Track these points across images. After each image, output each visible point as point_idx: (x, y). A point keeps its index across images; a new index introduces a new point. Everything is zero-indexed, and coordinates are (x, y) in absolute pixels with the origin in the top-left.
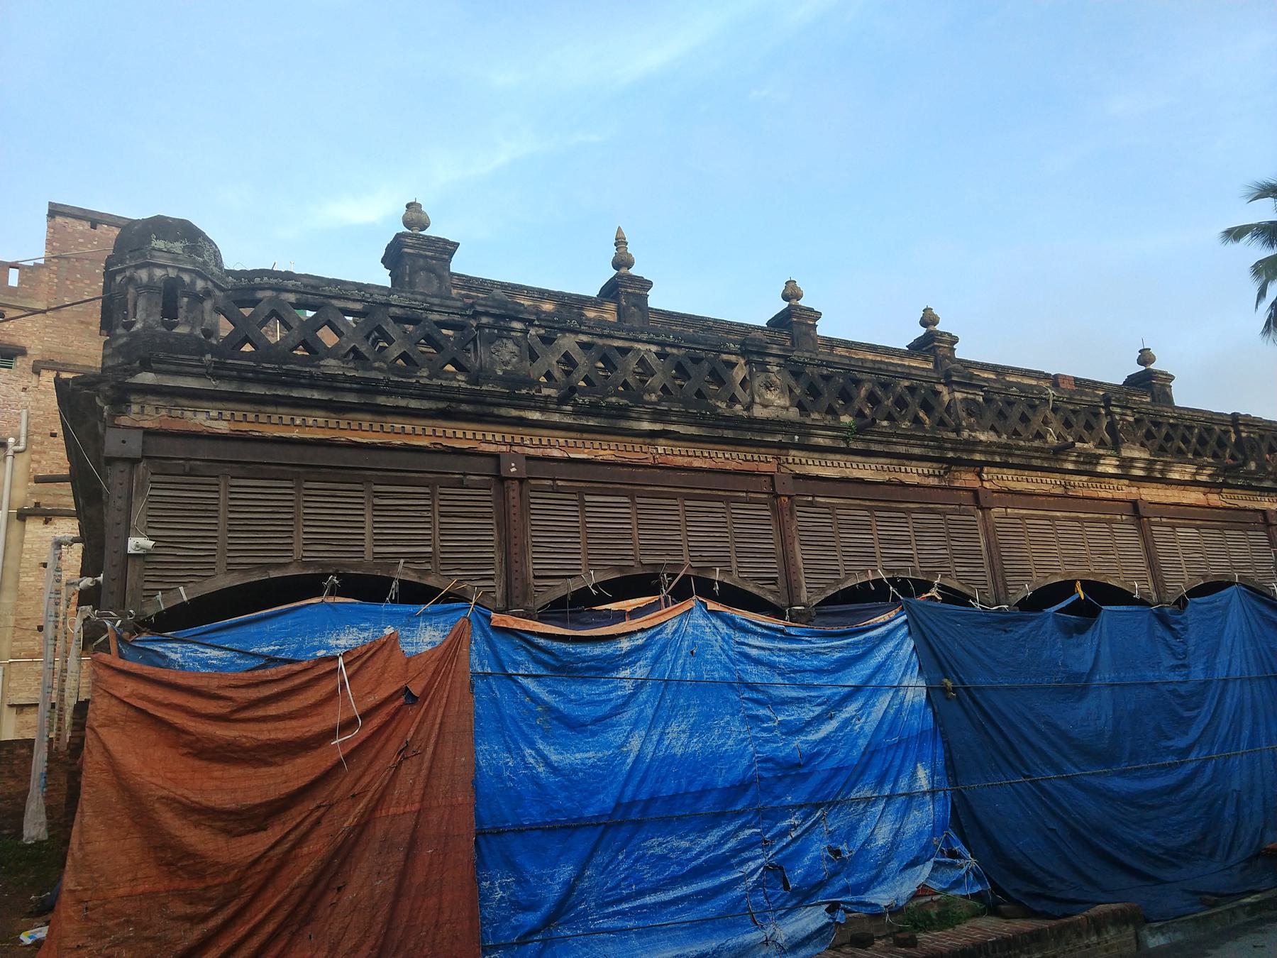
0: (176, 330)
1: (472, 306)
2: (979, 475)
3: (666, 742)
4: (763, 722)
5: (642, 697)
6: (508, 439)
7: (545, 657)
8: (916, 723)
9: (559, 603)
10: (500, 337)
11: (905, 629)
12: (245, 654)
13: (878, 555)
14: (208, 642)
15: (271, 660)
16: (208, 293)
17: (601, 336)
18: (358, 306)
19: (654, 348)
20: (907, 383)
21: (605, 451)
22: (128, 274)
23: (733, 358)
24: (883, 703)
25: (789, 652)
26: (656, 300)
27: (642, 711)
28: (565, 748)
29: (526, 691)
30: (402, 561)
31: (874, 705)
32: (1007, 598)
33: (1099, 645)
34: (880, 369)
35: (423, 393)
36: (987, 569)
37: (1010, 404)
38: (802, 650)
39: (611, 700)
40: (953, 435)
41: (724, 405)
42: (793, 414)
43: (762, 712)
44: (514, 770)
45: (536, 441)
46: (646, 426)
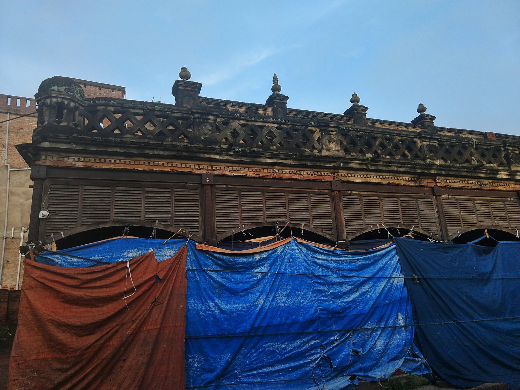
0: (61, 124)
1: (191, 109)
2: (435, 180)
3: (276, 301)
4: (323, 293)
5: (266, 280)
6: (206, 167)
7: (220, 262)
8: (398, 294)
9: (228, 239)
10: (203, 123)
11: (395, 251)
12: (88, 260)
13: (382, 217)
14: (73, 255)
15: (99, 263)
16: (76, 108)
17: (251, 121)
18: (141, 111)
19: (276, 125)
20: (399, 138)
21: (251, 172)
22: (42, 101)
23: (314, 129)
24: (382, 285)
25: (336, 261)
26: (290, 105)
27: (265, 287)
28: (228, 302)
29: (211, 277)
30: (157, 221)
31: (377, 286)
32: (447, 237)
33: (496, 260)
34: (386, 132)
35: (165, 148)
36: (438, 224)
37: (452, 146)
38: (343, 261)
39: (250, 282)
40: (422, 162)
41: (308, 150)
42: (342, 153)
43: (322, 288)
44: (205, 312)
45: (218, 168)
46: (268, 160)
